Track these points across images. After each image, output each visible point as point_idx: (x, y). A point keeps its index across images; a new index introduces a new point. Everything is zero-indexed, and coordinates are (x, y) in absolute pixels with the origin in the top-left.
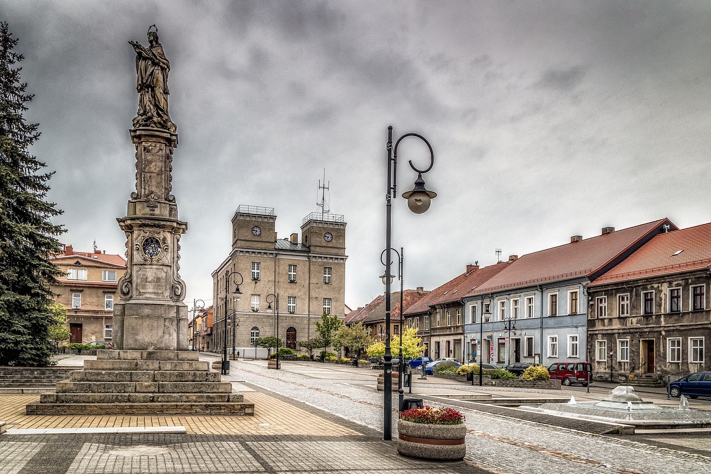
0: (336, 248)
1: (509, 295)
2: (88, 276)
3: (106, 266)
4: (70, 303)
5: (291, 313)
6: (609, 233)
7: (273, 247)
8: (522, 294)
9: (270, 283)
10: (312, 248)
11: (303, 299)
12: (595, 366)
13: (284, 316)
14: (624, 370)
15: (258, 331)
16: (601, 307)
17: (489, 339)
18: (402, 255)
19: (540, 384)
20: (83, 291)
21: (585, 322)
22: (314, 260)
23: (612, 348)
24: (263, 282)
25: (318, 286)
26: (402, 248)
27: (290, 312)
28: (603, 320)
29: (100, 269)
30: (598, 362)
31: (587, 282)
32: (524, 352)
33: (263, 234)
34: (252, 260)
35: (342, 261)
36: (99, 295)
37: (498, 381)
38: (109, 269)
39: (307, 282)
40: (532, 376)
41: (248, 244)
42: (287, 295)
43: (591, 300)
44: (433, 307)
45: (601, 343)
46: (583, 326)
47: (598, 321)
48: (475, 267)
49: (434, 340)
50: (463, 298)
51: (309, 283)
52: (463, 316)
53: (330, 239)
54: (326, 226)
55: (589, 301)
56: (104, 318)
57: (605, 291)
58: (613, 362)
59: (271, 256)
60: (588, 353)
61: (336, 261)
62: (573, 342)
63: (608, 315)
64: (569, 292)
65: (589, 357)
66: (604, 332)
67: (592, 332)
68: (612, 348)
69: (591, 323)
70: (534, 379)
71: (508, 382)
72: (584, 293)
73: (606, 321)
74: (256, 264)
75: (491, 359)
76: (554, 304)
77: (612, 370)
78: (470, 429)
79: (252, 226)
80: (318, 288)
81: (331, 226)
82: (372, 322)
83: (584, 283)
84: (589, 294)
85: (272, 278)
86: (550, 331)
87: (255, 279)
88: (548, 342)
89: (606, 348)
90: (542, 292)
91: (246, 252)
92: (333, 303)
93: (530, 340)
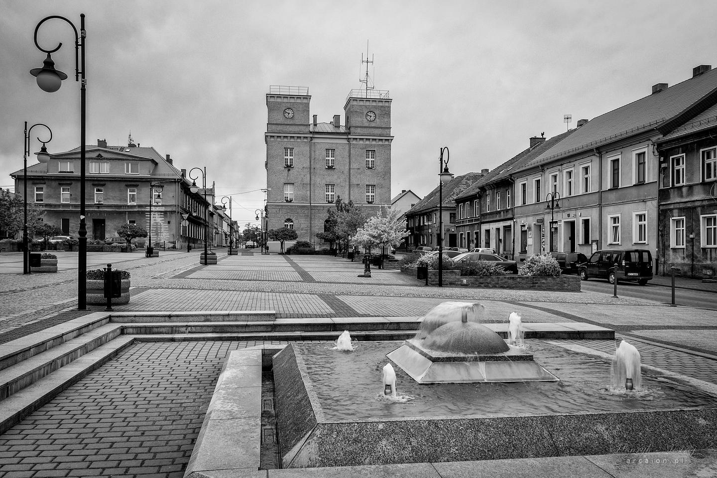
0: (380, 128)
1: (562, 165)
2: (110, 170)
3: (129, 158)
4: (92, 197)
5: (329, 202)
6: (702, 73)
7: (307, 130)
8: (577, 163)
9: (305, 170)
10: (352, 130)
11: (342, 186)
12: (669, 255)
13: (321, 206)
14: (711, 260)
15: (292, 223)
16: (678, 171)
17: (540, 224)
18: (83, 28)
19: (544, 283)
20: (138, 186)
21: (655, 194)
22: (354, 142)
23: (693, 228)
24: (297, 169)
25: (359, 171)
26: (83, 16)
27: (329, 201)
28: (680, 188)
29: (120, 162)
30: (674, 250)
31: (660, 137)
32: (580, 238)
33: (296, 116)
34: (285, 145)
35: (387, 143)
36: (122, 189)
37: (472, 279)
38: (131, 161)
39: (347, 167)
40: (532, 271)
41: (280, 128)
42: (324, 182)
43: (663, 162)
44: (483, 189)
45: (678, 222)
46: (652, 199)
47: (674, 191)
48: (540, 140)
49: (484, 227)
50: (511, 175)
51: (350, 169)
52: (513, 198)
53: (372, 118)
54: (368, 103)
55: (660, 163)
56: (127, 213)
57: (682, 146)
58: (695, 248)
59: (305, 140)
60: (660, 237)
61: (380, 143)
62: (641, 223)
63: (687, 180)
64: (634, 153)
65: (661, 242)
66: (682, 206)
67: (664, 208)
68: (693, 228)
69: (663, 194)
70: (534, 275)
71: (489, 280)
72: (653, 152)
73: (684, 190)
74: (289, 149)
75: (542, 249)
76: (616, 172)
77: (693, 260)
78: (350, 363)
79: (284, 108)
80: (360, 174)
81: (374, 104)
82: (427, 211)
83: (654, 139)
84: (661, 154)
85: (307, 164)
86: (611, 209)
87: (288, 166)
88: (610, 224)
89: (685, 228)
90: (601, 157)
91: (278, 136)
92: (378, 191)
93: (586, 222)
